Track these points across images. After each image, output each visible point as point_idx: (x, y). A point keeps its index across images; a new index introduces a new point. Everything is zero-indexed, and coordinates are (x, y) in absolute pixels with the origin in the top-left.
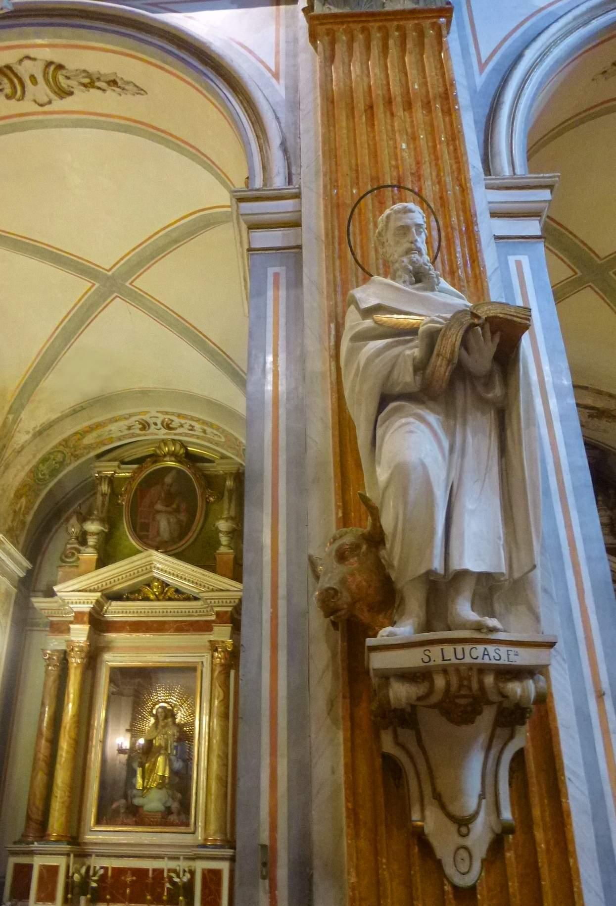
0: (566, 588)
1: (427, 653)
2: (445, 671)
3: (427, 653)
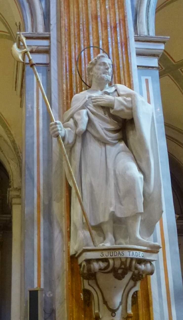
0: (27, 310)
1: (102, 253)
2: (113, 259)
3: (102, 253)
